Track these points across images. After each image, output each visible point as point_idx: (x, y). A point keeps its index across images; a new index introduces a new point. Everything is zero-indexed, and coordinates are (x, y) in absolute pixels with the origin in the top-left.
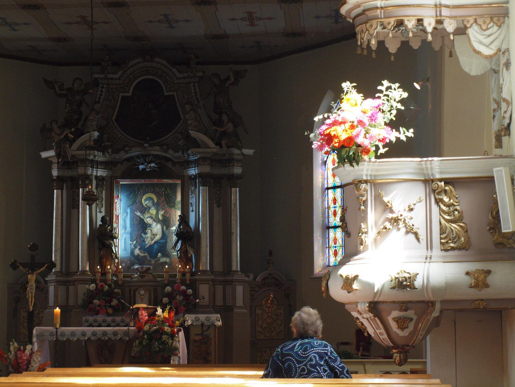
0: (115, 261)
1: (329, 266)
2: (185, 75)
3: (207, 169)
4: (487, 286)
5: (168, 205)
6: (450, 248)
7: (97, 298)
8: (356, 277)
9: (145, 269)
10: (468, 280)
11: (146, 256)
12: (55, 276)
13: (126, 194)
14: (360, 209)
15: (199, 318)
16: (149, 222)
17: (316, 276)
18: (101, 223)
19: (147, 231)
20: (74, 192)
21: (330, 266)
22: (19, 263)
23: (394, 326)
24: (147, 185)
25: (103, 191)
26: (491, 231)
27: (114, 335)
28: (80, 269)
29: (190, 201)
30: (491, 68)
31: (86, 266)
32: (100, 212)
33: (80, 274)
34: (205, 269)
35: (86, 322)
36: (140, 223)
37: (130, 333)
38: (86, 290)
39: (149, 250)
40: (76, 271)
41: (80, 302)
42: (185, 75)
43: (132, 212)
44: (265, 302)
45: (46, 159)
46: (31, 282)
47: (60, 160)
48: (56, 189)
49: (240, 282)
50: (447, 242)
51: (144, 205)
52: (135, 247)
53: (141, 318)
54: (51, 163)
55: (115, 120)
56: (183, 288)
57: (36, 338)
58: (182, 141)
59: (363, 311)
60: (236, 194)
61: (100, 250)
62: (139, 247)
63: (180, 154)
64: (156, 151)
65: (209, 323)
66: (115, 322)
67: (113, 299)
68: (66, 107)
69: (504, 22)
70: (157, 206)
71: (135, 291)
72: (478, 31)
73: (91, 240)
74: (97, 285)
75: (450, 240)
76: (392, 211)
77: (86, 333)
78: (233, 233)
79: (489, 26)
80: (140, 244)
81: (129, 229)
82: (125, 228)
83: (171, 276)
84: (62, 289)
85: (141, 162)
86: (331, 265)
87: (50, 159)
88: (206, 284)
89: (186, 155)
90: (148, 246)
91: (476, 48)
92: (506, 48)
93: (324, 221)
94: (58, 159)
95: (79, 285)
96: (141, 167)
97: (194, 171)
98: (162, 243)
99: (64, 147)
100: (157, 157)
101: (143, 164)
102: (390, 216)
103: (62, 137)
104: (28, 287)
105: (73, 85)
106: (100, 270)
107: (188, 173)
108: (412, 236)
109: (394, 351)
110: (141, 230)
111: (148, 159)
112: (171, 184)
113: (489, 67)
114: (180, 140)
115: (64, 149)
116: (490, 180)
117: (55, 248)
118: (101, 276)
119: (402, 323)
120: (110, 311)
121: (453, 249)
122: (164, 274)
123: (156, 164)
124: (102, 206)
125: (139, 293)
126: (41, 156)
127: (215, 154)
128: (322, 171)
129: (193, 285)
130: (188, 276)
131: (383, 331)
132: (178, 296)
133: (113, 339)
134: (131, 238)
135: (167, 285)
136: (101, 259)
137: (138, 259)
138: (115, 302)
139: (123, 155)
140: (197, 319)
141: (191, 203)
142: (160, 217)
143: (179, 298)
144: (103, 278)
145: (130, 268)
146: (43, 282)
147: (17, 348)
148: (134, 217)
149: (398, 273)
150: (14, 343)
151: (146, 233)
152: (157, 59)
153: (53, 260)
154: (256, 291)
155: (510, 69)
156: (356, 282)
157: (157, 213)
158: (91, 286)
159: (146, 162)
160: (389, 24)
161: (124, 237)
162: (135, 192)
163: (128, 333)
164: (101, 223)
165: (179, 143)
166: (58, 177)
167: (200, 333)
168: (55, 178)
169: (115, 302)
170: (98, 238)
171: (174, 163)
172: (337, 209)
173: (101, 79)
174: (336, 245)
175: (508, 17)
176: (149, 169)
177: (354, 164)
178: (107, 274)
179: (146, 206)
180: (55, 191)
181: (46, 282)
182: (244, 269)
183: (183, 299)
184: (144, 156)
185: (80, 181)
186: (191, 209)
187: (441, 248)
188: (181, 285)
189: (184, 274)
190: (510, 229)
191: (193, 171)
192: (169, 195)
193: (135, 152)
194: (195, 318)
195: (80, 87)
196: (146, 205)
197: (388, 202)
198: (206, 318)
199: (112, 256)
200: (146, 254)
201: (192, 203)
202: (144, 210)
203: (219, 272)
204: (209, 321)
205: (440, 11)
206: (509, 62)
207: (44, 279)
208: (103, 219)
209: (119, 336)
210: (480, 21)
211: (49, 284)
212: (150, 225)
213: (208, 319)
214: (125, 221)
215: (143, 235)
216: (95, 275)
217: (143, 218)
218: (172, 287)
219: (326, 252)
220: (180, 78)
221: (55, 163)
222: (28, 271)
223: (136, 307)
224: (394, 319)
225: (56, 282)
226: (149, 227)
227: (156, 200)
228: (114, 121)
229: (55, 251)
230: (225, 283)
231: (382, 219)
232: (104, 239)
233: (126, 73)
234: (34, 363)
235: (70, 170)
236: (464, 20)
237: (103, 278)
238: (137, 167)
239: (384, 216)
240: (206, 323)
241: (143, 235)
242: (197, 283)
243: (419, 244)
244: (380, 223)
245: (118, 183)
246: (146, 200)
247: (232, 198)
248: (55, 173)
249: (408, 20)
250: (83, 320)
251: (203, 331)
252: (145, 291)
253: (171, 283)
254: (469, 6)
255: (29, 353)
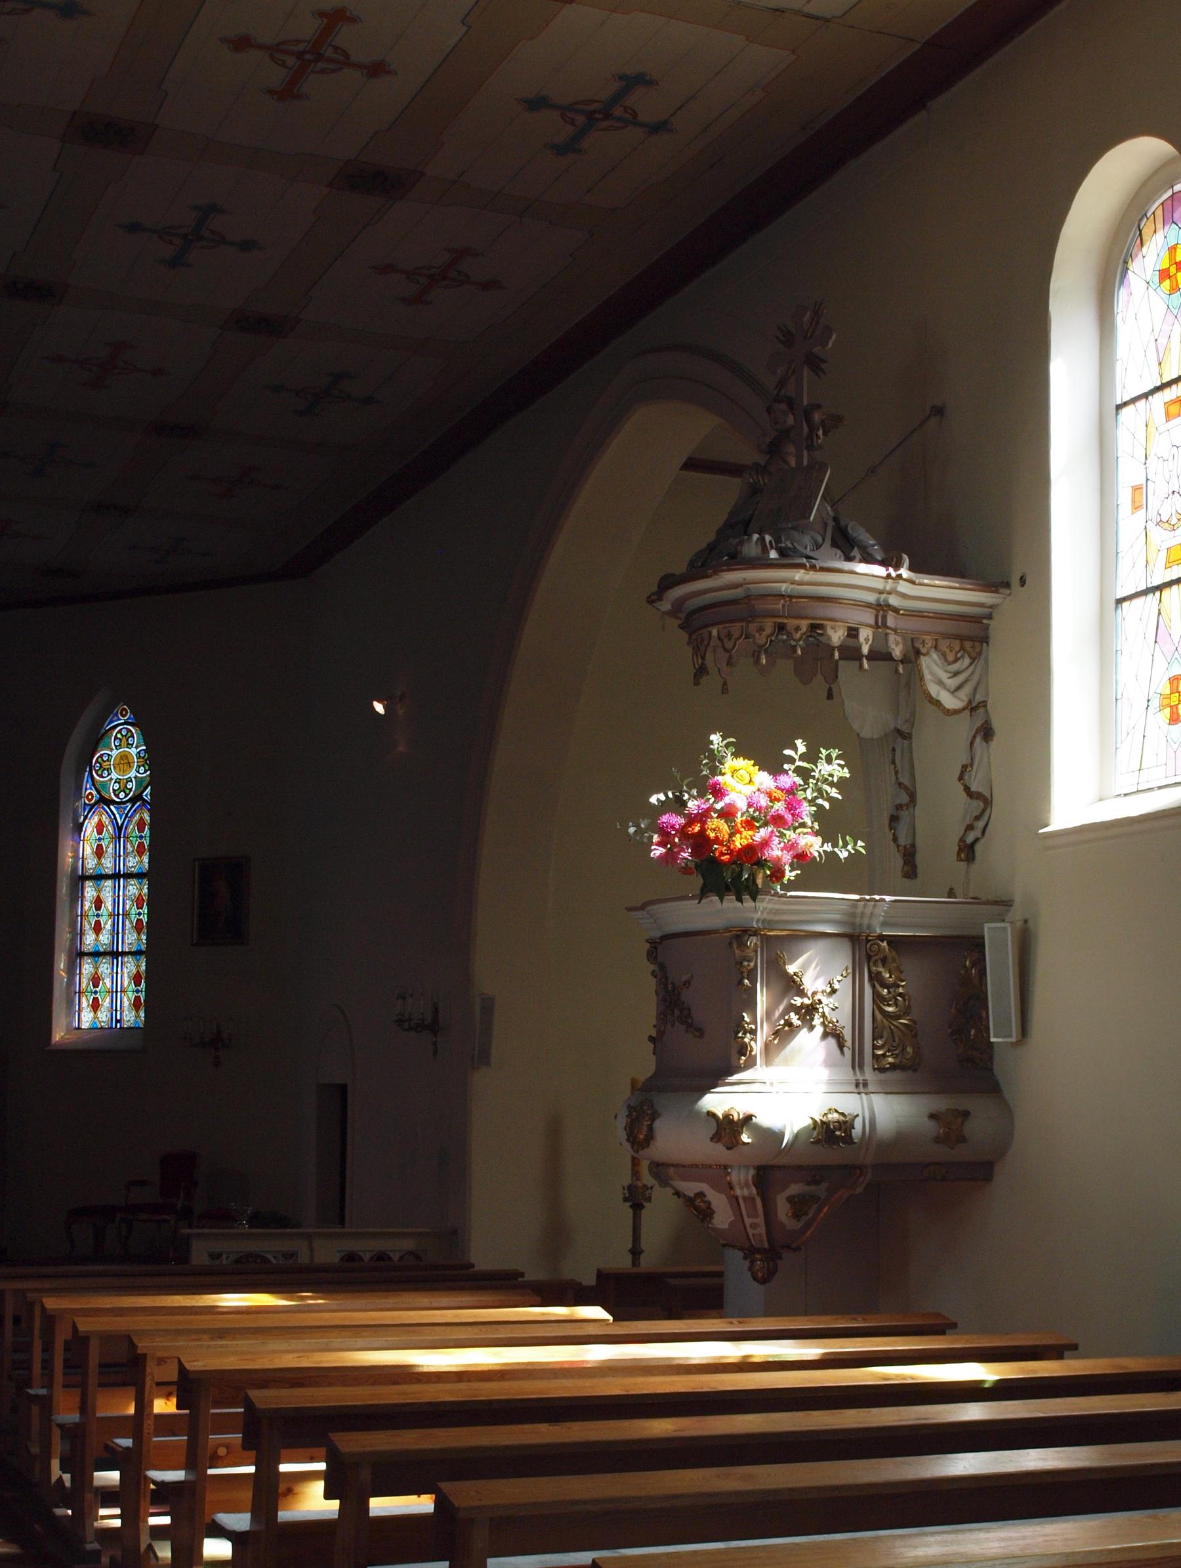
1: (79, 1028)
4: (962, 1139)
6: (888, 1066)
8: (748, 1118)
10: (931, 1128)
14: (741, 982)
21: (81, 1029)
23: (783, 1210)
26: (954, 1038)
30: (895, 728)
50: (884, 1055)
59: (740, 1184)
69: (980, 654)
72: (939, 662)
75: (889, 1051)
76: (802, 993)
79: (959, 655)
86: (83, 1027)
91: (934, 694)
92: (983, 699)
102: (798, 1001)
108: (832, 1041)
109: (758, 1256)
113: (892, 727)
116: (976, 944)
119: (799, 1205)
121: (893, 1067)
128: (74, 843)
131: (760, 1220)
149: (825, 1114)
155: (992, 740)
156: (746, 1129)
160: (797, 629)
172: (102, 920)
174: (98, 989)
175: (987, 643)
177: (746, 897)
187: (873, 1066)
190: (1011, 1036)
197: (795, 975)
205: (884, 618)
206: (989, 726)
210: (944, 644)
224: (790, 1200)
231: (781, 1008)
236: (915, 640)
239: (785, 1002)
243: (842, 1057)
244: (777, 1014)
249: (832, 628)
254: (925, 614)
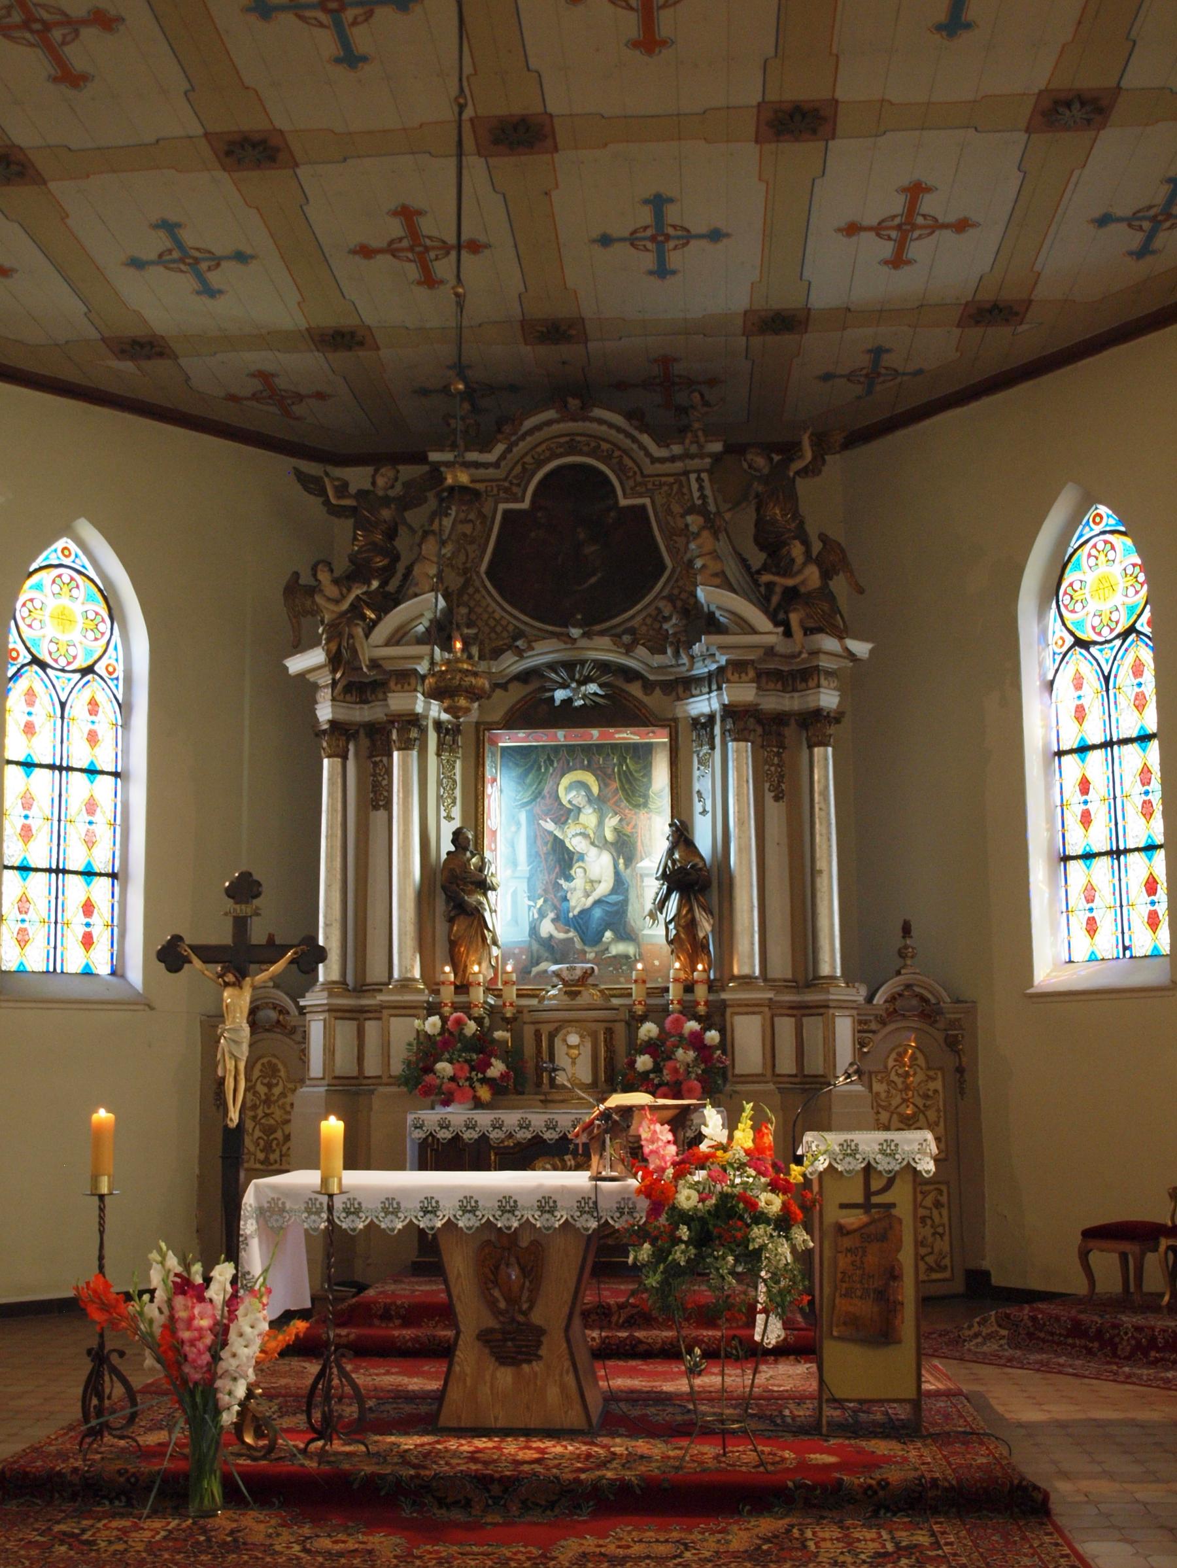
0: (490, 954)
2: (677, 449)
3: (745, 693)
5: (628, 801)
7: (447, 1056)
9: (578, 973)
11: (571, 940)
12: (325, 994)
13: (514, 774)
15: (857, 1145)
16: (578, 849)
17: (1039, 990)
18: (453, 849)
19: (572, 872)
20: (375, 764)
22: (190, 947)
24: (571, 749)
25: (455, 762)
27: (543, 1212)
28: (396, 975)
29: (697, 786)
31: (413, 967)
32: (449, 818)
33: (395, 986)
34: (746, 971)
35: (416, 1128)
36: (554, 849)
37: (600, 1204)
38: (414, 1035)
39: (580, 923)
40: (386, 980)
41: (397, 1068)
42: (677, 449)
43: (533, 820)
44: (896, 1060)
45: (302, 676)
46: (234, 1017)
47: (338, 675)
48: (329, 757)
49: (842, 1006)
51: (565, 802)
52: (542, 915)
53: (652, 1152)
54: (315, 687)
55: (487, 573)
56: (692, 1025)
57: (254, 1222)
58: (674, 621)
60: (824, 762)
61: (451, 921)
62: (552, 915)
63: (667, 658)
64: (601, 650)
65: (893, 1163)
66: (500, 1128)
67: (493, 1060)
68: (355, 539)
70: (599, 802)
71: (552, 1037)
73: (424, 896)
74: (444, 1020)
77: (437, 1202)
78: (821, 872)
80: (555, 908)
81: (524, 867)
82: (515, 864)
83: (651, 992)
84: (345, 1030)
85: (560, 680)
87: (311, 677)
88: (754, 1013)
89: (685, 659)
90: (576, 912)
93: (1052, 841)
94: (334, 671)
95: (392, 1019)
96: (560, 695)
97: (706, 703)
98: (615, 904)
99: (351, 636)
100: (604, 667)
101: (564, 686)
103: (345, 606)
104: (222, 1034)
105: (374, 483)
106: (452, 976)
107: (685, 711)
110: (557, 869)
111: (581, 674)
112: (636, 747)
114: (667, 619)
115: (351, 641)
117: (325, 917)
118: (456, 993)
120: (484, 1093)
122: (633, 986)
123: (601, 686)
124: (454, 802)
125: (565, 1041)
126: (287, 668)
127: (770, 651)
129: (716, 1016)
130: (701, 992)
132: (680, 1051)
133: (538, 1225)
134: (529, 890)
135: (643, 1019)
136: (453, 945)
137: (554, 950)
138: (497, 1068)
139: (510, 664)
140: (850, 1151)
141: (699, 792)
142: (609, 836)
143: (685, 1056)
144: (462, 999)
145: (530, 972)
146: (294, 1011)
147: (176, 1275)
148: (537, 834)
150: (164, 1256)
151: (569, 878)
152: (598, 412)
153: (321, 943)
154: (874, 1032)
157: (601, 823)
158: (427, 1023)
159: (573, 679)
161: (512, 890)
162: (540, 768)
163: (595, 1203)
164: (453, 849)
165: (666, 626)
166: (332, 723)
167: (859, 1199)
168: (326, 727)
169: (497, 1068)
170: (444, 888)
171: (648, 686)
173: (448, 464)
176: (582, 702)
178: (472, 990)
179: (569, 806)
180: (326, 761)
181: (302, 1011)
182: (850, 976)
183: (696, 1059)
184: (569, 666)
185: (394, 732)
186: (698, 807)
188: (684, 1018)
189: (689, 988)
191: (703, 704)
192: (631, 773)
193: (543, 654)
194: (841, 1145)
195: (392, 487)
196: (570, 802)
198: (881, 1144)
199: (484, 939)
200: (571, 934)
201: (702, 791)
202: (564, 815)
203: (785, 981)
204: (892, 1155)
207: (297, 1003)
208: (457, 836)
209: (562, 1216)
211: (309, 1017)
212: (581, 857)
213: (888, 1150)
214: (513, 845)
215: (562, 882)
216: (437, 992)
217: (561, 837)
218: (660, 1025)
219: (1059, 924)
220: (662, 460)
221: (326, 686)
222: (221, 976)
223: (617, 1107)
225: (329, 1011)
226: (578, 861)
227: (595, 790)
228: (484, 576)
229: (326, 925)
230: (801, 1011)
232: (463, 890)
233: (515, 450)
234: (241, 1341)
235: (366, 706)
237: (462, 999)
238: (548, 694)
240: (884, 1164)
241: (562, 882)
242: (729, 1011)
245: (494, 743)
246: (568, 789)
247: (816, 777)
248: (325, 712)
250: (409, 1122)
251: (868, 1193)
252: (582, 1037)
253: (658, 1013)
255: (221, 1297)
